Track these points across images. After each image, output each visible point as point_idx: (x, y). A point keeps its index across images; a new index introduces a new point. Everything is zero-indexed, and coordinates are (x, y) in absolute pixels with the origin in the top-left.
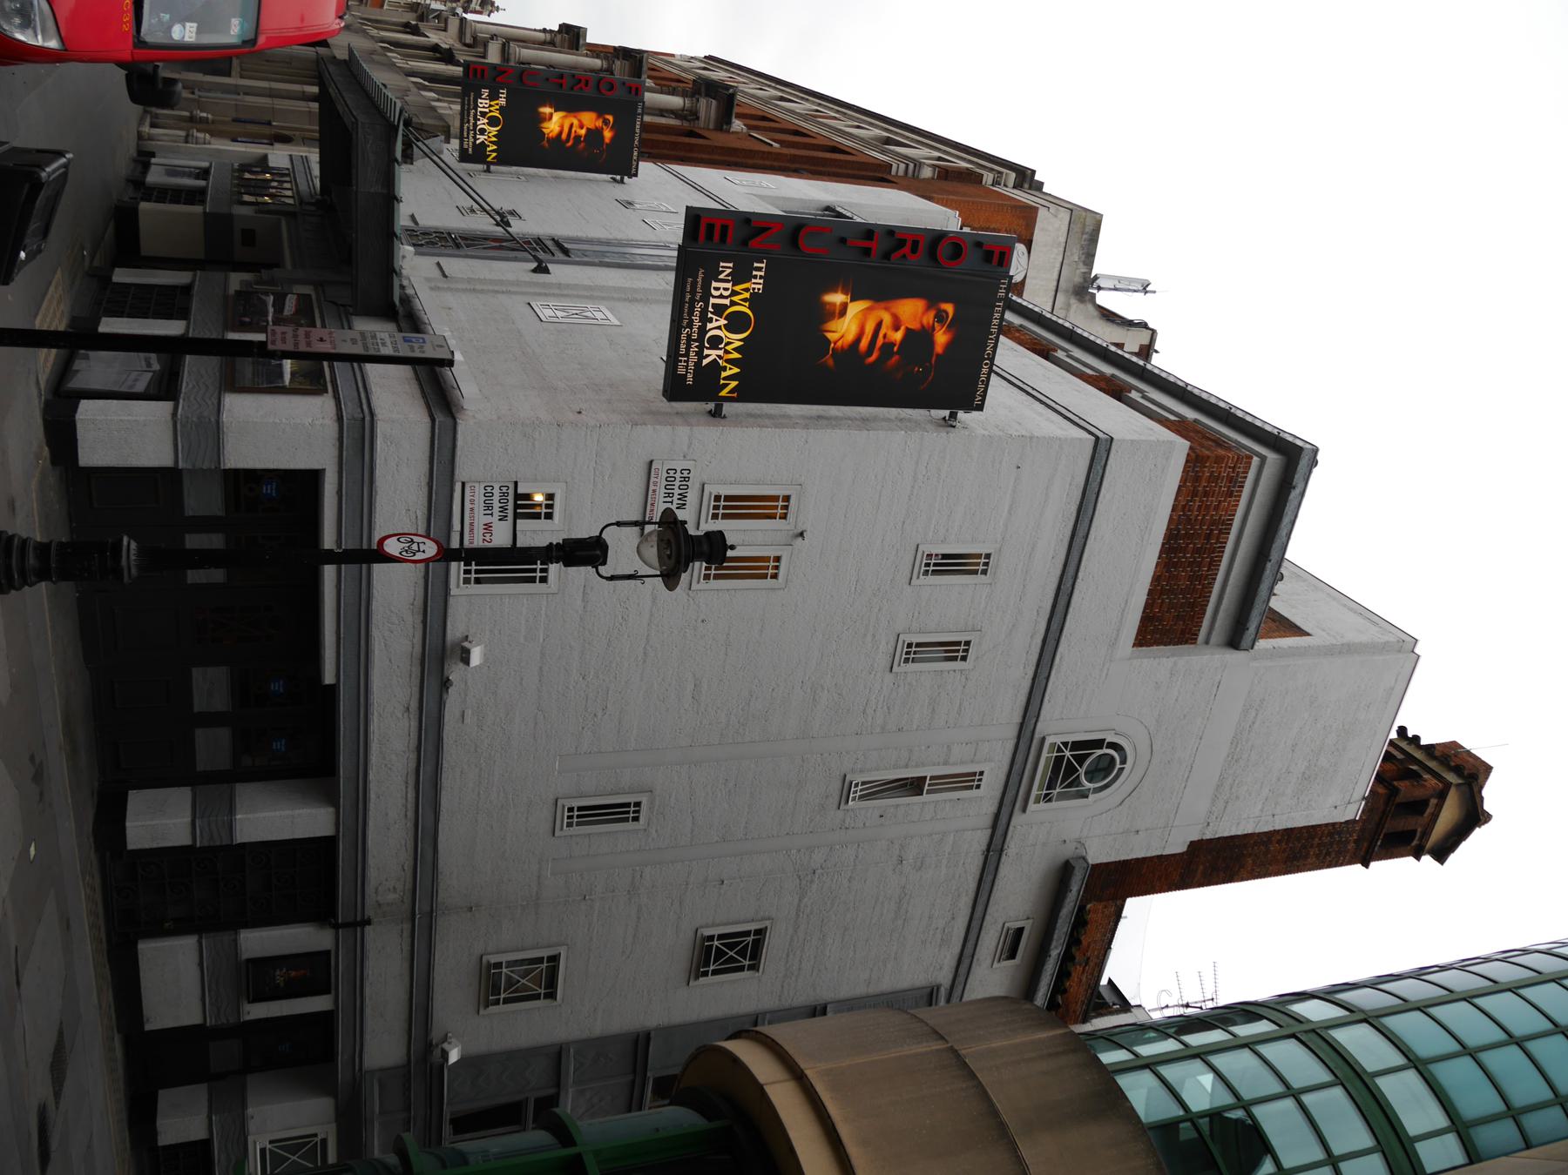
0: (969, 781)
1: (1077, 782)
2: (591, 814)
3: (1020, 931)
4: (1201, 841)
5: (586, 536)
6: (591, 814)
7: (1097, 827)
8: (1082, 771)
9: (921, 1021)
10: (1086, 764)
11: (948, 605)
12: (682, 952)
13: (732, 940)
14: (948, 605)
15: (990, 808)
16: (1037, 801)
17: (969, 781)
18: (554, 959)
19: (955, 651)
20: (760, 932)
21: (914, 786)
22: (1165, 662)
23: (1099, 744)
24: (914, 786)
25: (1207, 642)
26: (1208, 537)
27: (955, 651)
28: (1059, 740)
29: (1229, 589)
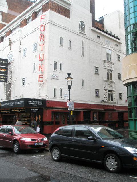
0: (82, 41)
1: (83, 27)
2: (83, 85)
3: (98, 36)
4: (92, 25)
5: (32, 98)
6: (83, 85)
7: (88, 25)
8: (83, 27)
9: (35, 172)
10: (82, 26)
11: (65, 43)
12: (96, 75)
13: (95, 70)
14: (65, 43)
15: (85, 39)
16: (85, 33)
17: (82, 41)
18: (95, 67)
19: (70, 42)
20: (95, 67)
21: (83, 47)
22: (72, 14)
23: (80, 24)
24: (83, 47)
25: (70, 8)
26: (59, 7)
27: (70, 42)
28: (79, 30)
29: (63, 4)
